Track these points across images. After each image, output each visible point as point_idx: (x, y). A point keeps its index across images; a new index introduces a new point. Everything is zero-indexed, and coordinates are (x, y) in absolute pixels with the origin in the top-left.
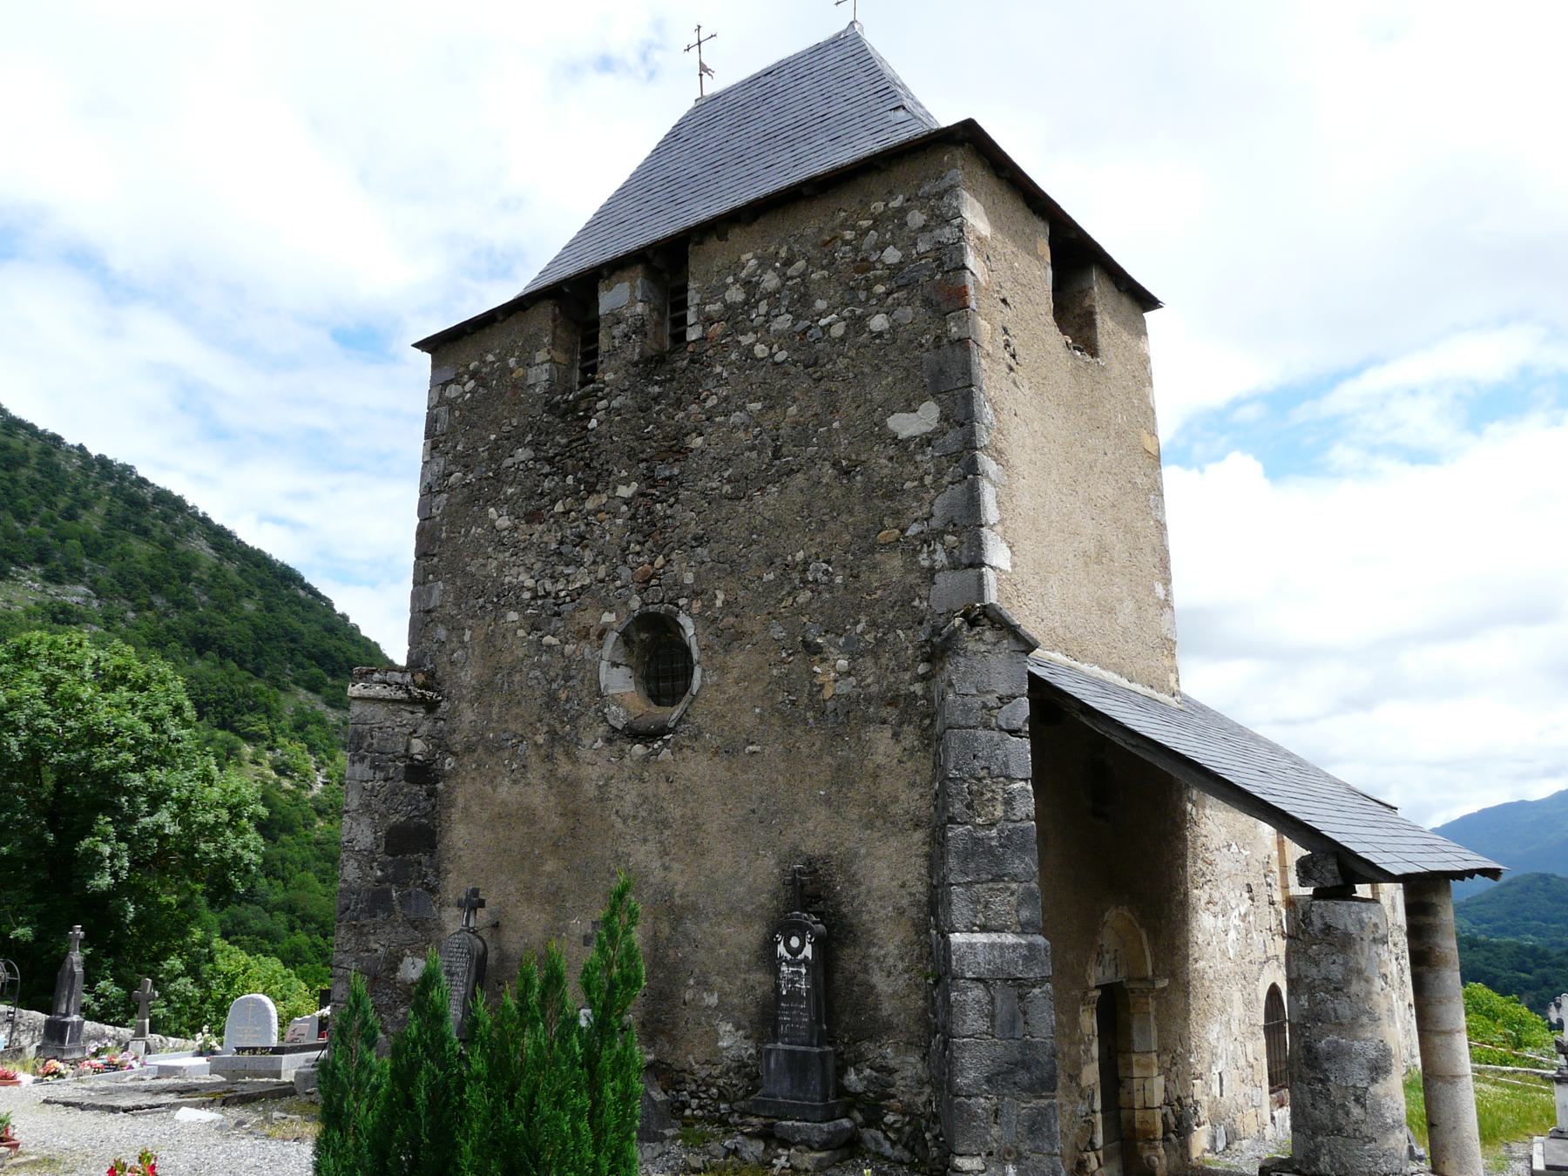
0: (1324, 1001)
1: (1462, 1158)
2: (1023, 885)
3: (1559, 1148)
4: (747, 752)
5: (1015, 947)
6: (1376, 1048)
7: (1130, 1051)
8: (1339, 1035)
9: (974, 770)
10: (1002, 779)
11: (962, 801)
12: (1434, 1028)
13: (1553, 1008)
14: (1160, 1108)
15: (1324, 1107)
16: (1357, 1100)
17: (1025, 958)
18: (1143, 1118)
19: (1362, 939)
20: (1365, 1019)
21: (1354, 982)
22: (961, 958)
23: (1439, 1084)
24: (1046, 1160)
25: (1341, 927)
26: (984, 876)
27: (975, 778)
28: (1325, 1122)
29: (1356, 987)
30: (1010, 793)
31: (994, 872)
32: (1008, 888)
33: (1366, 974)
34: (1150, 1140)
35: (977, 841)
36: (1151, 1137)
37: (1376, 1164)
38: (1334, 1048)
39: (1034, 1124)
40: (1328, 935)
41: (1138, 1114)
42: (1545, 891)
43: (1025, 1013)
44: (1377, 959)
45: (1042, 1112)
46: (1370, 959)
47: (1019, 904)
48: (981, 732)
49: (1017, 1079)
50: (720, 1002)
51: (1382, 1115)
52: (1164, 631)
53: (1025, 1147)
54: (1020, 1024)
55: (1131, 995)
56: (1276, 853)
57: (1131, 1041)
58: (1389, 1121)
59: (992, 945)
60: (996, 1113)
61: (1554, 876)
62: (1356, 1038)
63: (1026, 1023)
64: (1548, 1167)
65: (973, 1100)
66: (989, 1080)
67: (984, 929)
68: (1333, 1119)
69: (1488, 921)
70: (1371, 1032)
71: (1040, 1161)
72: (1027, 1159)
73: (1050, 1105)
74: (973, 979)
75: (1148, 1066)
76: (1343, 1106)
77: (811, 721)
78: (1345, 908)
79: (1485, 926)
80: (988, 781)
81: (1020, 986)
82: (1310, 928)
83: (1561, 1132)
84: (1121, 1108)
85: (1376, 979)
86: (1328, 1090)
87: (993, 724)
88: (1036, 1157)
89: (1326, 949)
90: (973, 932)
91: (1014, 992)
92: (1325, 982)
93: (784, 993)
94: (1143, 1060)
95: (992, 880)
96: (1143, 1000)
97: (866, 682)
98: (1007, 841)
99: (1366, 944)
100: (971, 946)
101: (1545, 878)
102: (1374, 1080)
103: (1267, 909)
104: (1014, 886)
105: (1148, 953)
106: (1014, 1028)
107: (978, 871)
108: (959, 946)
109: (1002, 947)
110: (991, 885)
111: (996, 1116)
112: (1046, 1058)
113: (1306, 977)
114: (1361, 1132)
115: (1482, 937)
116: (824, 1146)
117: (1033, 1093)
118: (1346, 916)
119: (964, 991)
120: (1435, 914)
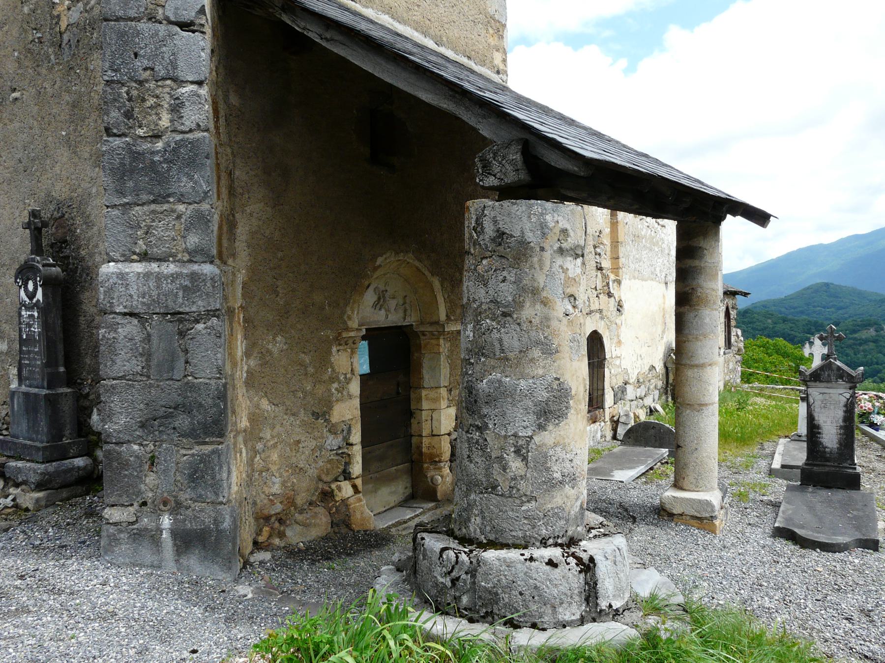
0: (489, 330)
1: (700, 474)
2: (191, 207)
3: (795, 449)
4: (11, 100)
5: (174, 277)
6: (549, 388)
7: (420, 387)
8: (503, 372)
9: (135, 71)
10: (168, 82)
11: (119, 109)
12: (688, 362)
13: (807, 345)
14: (449, 434)
15: (479, 460)
16: (517, 452)
17: (185, 289)
18: (430, 443)
19: (542, 249)
20: (536, 353)
21: (528, 304)
22: (110, 290)
23: (688, 412)
24: (209, 509)
25: (517, 234)
26: (144, 197)
27: (136, 81)
28: (480, 477)
29: (529, 311)
30: (178, 98)
31: (156, 191)
32: (173, 211)
33: (544, 294)
34: (436, 461)
35: (137, 156)
36: (437, 459)
37: (534, 527)
38: (496, 389)
39: (196, 472)
40: (500, 244)
41: (426, 441)
42: (826, 292)
43: (186, 351)
44: (562, 276)
45: (204, 459)
46: (551, 275)
47: (187, 229)
48: (143, 26)
49: (177, 424)
50: (9, 347)
51: (548, 469)
52: (491, 11)
53: (185, 496)
54: (180, 364)
55: (422, 337)
56: (608, 230)
57: (421, 378)
58: (557, 475)
59: (147, 275)
60: (152, 461)
61: (832, 284)
62: (523, 377)
63: (187, 362)
64: (783, 466)
65: (124, 448)
66: (143, 425)
67: (144, 257)
68: (488, 475)
69: (795, 308)
70: (544, 367)
71: (202, 511)
72: (187, 508)
73: (214, 452)
74: (125, 314)
75: (436, 400)
76: (500, 459)
77: (52, 57)
78: (524, 208)
79: (793, 310)
80: (152, 85)
81: (181, 321)
82: (481, 237)
83: (800, 436)
84: (412, 436)
85: (559, 302)
86: (486, 440)
87: (160, 17)
88: (198, 506)
89: (496, 263)
90: (133, 261)
91: (172, 328)
92: (492, 306)
93: (24, 337)
94: (432, 394)
95: (154, 202)
96: (434, 342)
97: (90, 6)
98: (173, 153)
99: (547, 255)
100: (122, 276)
101: (827, 285)
102: (541, 427)
103: (594, 272)
104: (181, 208)
105: (441, 300)
106: (172, 369)
107: (137, 191)
108: (108, 277)
109: (159, 277)
110: (153, 207)
111: (152, 464)
112: (210, 401)
113: (475, 301)
114: (518, 490)
115: (790, 317)
116: (39, 487)
117: (195, 438)
118: (525, 219)
119: (113, 327)
120: (701, 257)
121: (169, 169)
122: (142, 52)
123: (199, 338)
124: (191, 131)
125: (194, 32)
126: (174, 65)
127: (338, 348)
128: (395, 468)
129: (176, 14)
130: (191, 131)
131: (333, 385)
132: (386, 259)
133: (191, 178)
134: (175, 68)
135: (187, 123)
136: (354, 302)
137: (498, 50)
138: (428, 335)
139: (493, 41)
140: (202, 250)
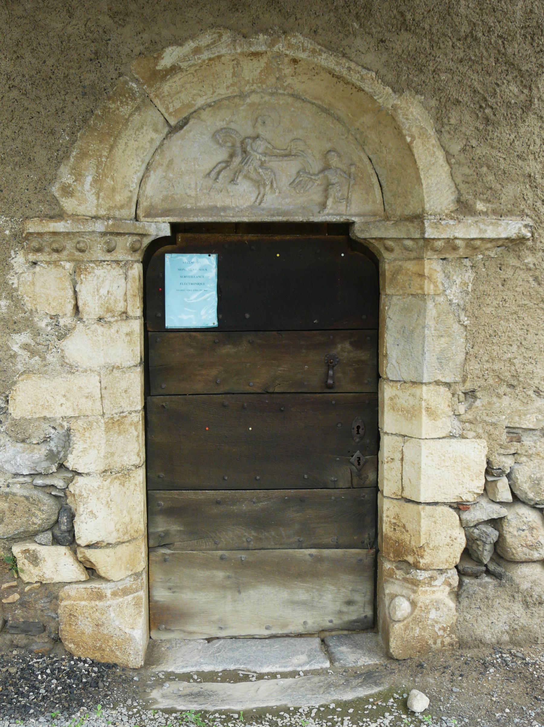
18: (397, 517)
36: (410, 559)
96: (410, 266)
127: (32, 257)
128: (313, 551)
131: (16, 337)
132: (197, 51)
136: (83, 155)
138: (397, 250)
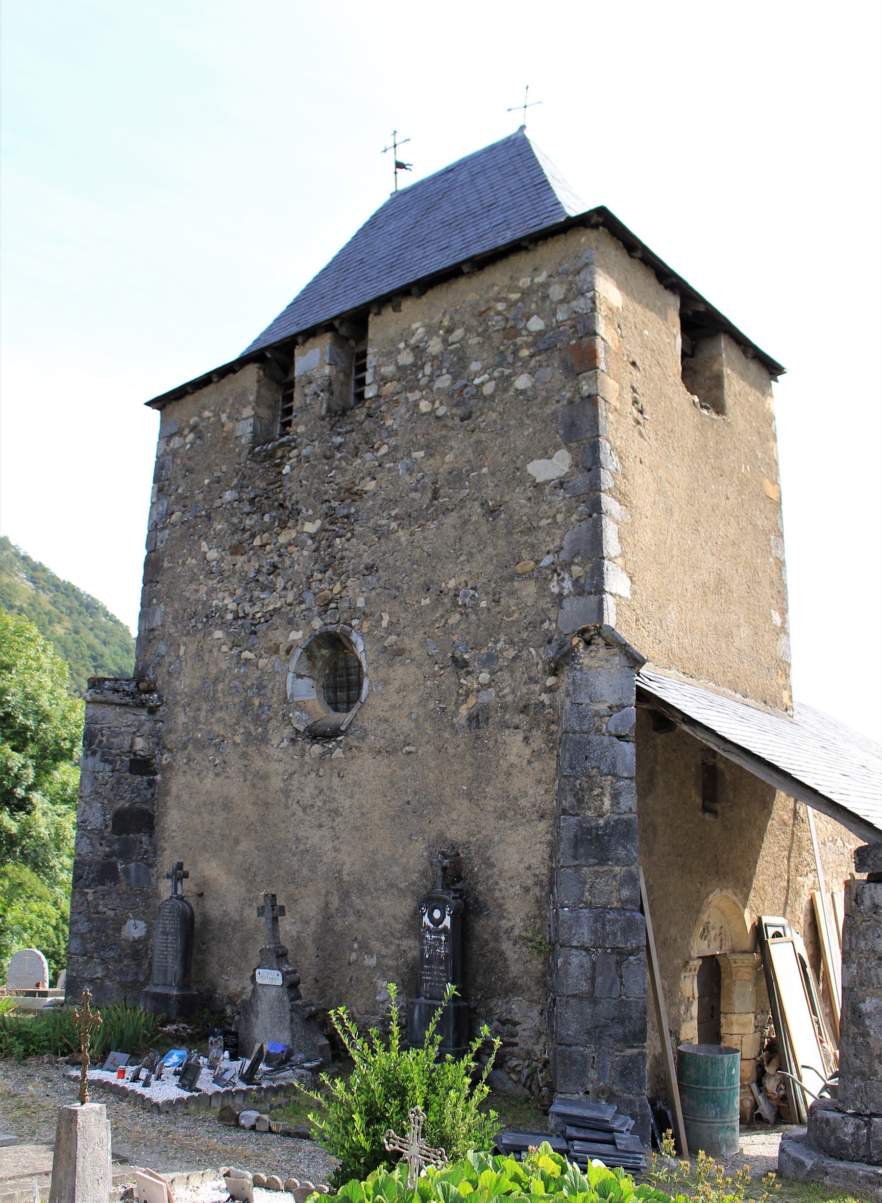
10: (609, 777)
20: (251, 941)
26: (592, 861)
39: (626, 1069)
45: (632, 1059)
73: (640, 1054)
95: (597, 864)
104: (617, 869)
110: (596, 868)
121: (609, 841)
122: (591, 756)
123: (631, 967)
124: (625, 812)
125: (627, 742)
126: (614, 765)
129: (616, 729)
130: (625, 812)
133: (625, 847)
134: (614, 767)
135: (623, 807)
137: (785, 689)
139: (781, 682)
140: (632, 901)
